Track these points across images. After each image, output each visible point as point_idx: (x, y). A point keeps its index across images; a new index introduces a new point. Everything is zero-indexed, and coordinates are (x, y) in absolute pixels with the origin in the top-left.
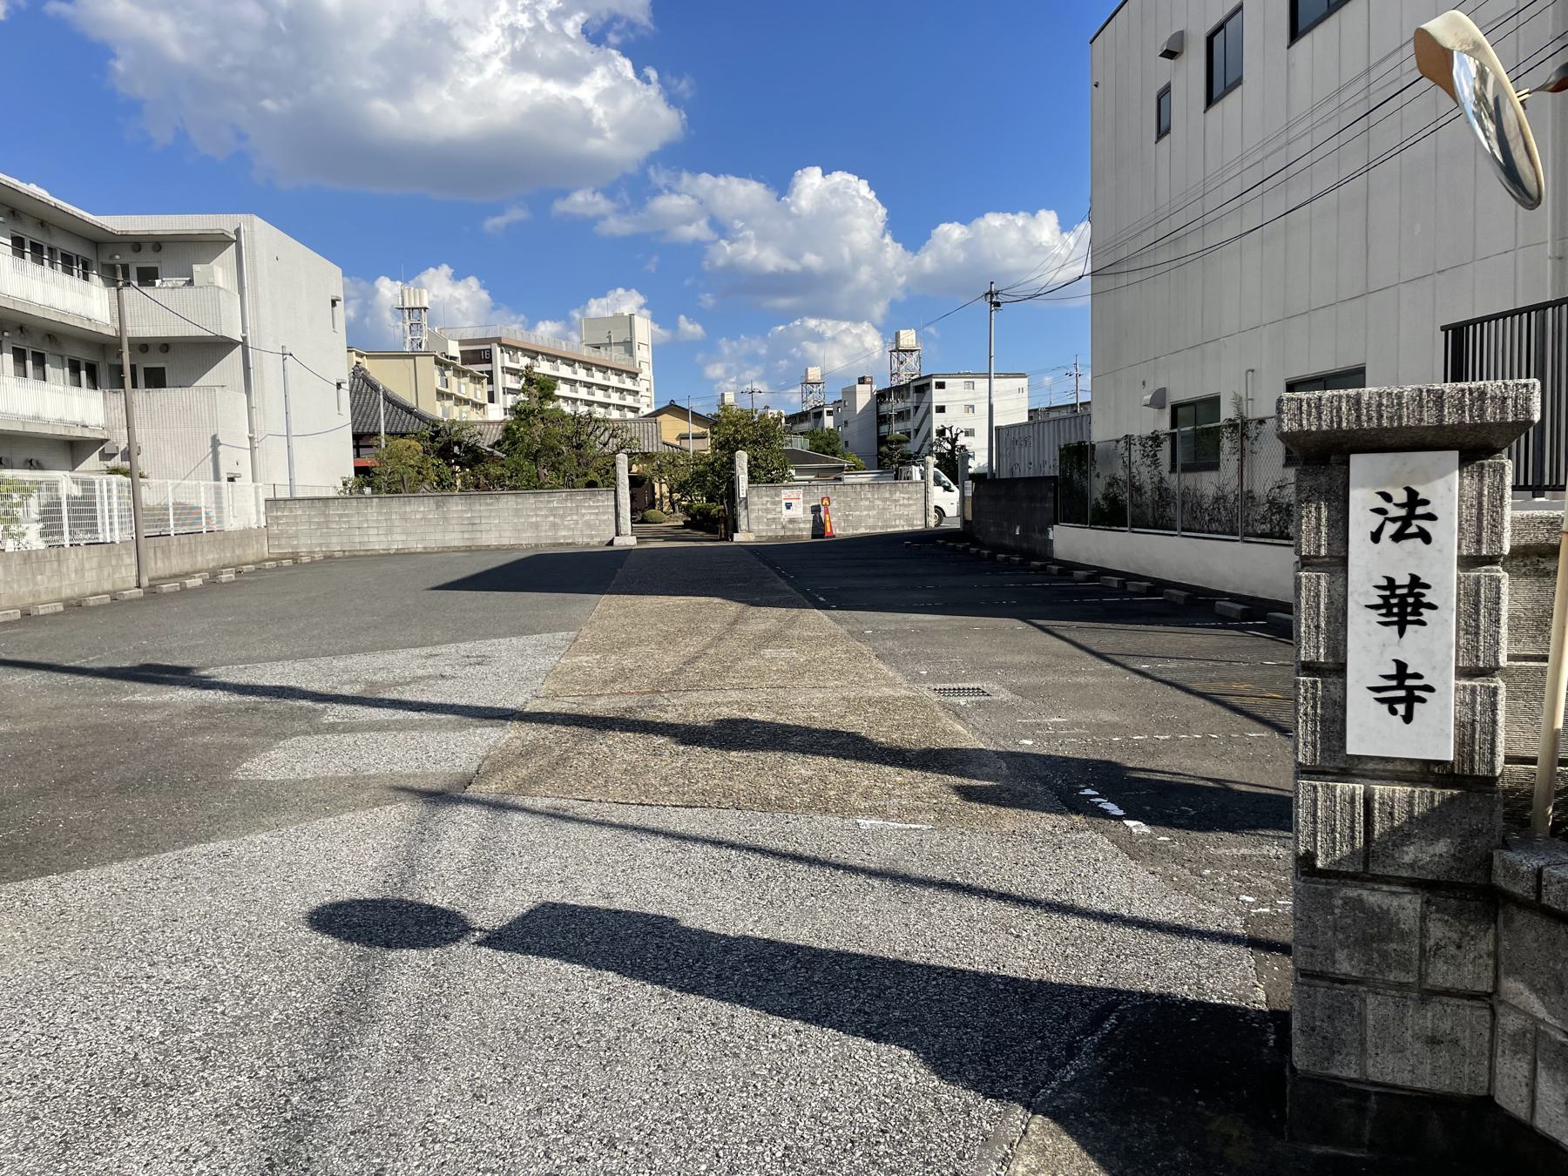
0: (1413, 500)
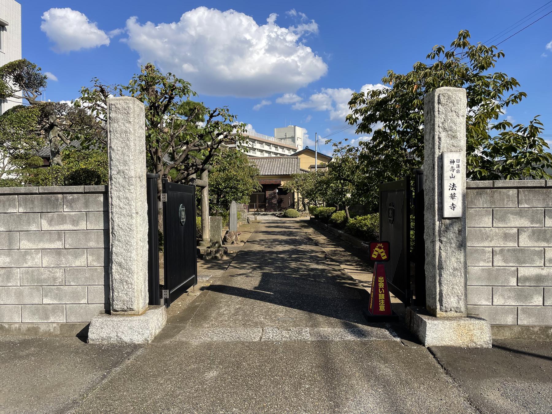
0: (454, 185)
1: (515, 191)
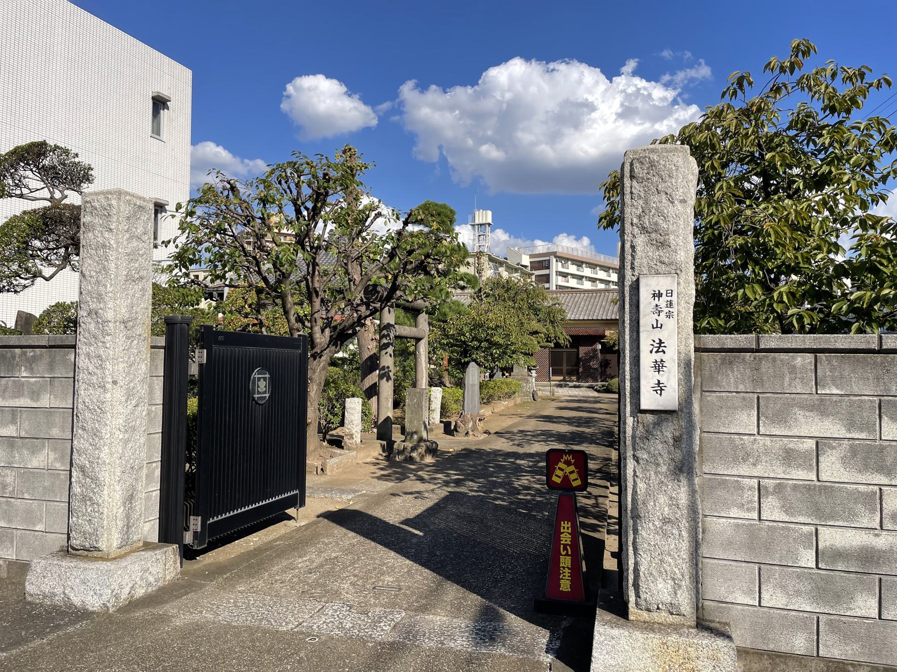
0: (661, 342)
1: (810, 357)
